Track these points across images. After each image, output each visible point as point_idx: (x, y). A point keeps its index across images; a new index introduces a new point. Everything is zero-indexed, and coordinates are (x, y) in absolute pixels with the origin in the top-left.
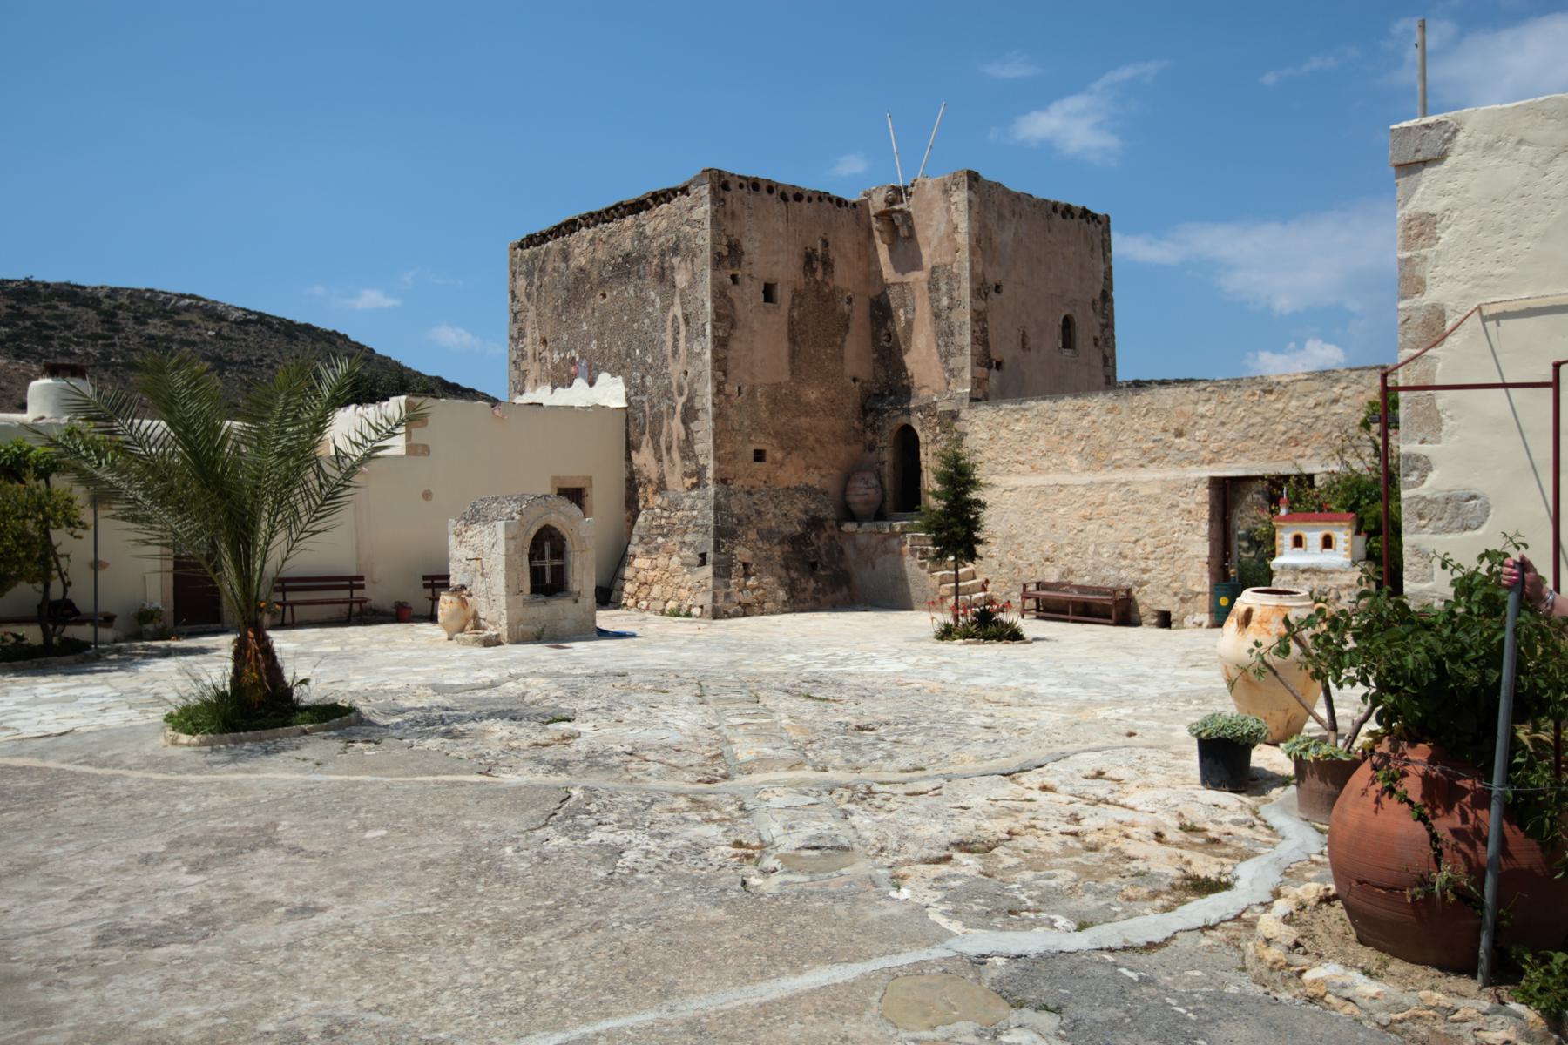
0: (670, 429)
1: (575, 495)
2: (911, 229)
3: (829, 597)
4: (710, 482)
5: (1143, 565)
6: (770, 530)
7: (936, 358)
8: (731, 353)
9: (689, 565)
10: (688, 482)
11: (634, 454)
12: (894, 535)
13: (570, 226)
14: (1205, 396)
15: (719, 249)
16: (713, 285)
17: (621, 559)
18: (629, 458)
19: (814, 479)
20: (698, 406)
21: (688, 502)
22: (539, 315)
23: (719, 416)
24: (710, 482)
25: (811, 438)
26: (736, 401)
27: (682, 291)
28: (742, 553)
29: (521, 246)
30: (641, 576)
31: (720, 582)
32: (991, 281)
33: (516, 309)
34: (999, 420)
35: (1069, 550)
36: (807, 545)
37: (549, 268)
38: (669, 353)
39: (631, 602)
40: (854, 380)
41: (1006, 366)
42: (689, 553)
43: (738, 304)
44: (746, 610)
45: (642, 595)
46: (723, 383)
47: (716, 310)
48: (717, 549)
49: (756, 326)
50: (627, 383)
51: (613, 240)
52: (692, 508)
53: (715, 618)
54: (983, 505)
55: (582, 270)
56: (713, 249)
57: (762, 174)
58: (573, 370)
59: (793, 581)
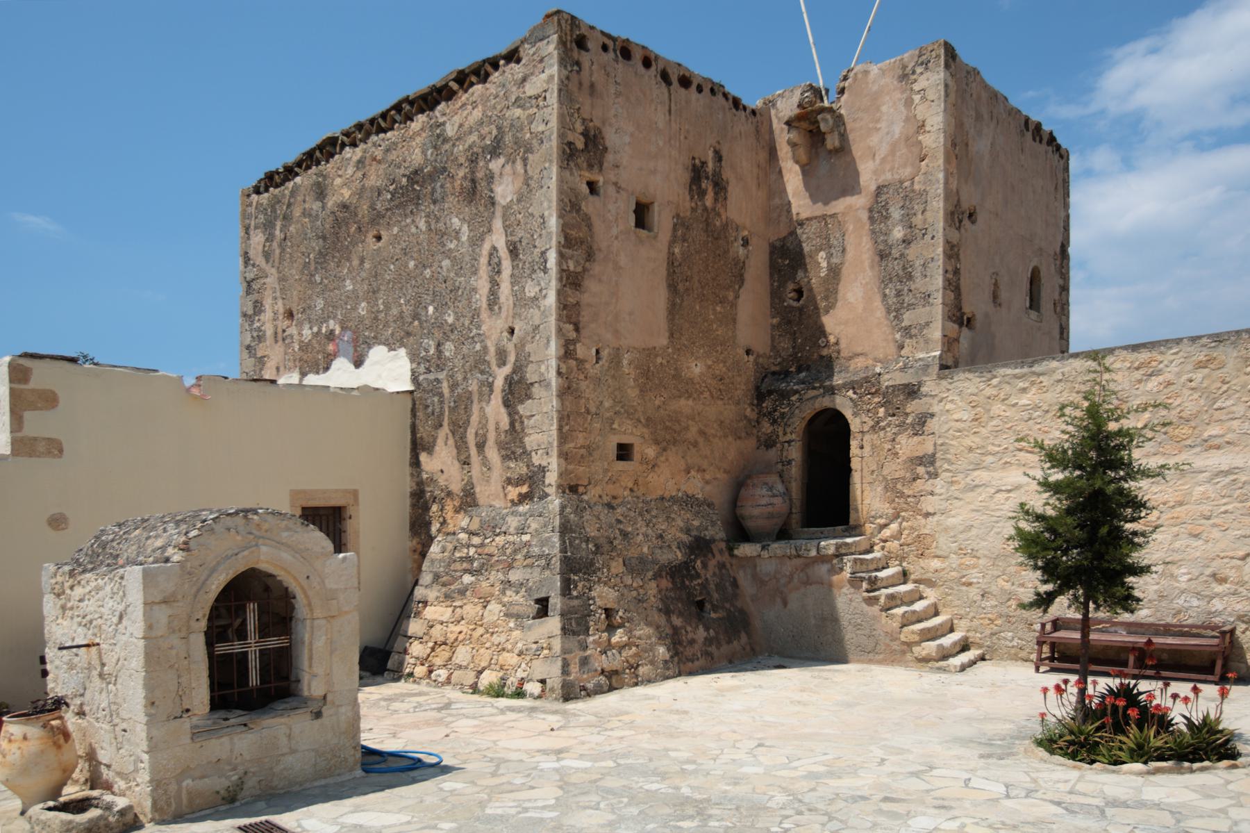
0: (484, 418)
1: (329, 520)
2: (843, 137)
3: (725, 649)
4: (551, 490)
6: (642, 560)
7: (880, 312)
8: (585, 298)
9: (518, 616)
10: (513, 493)
11: (423, 457)
12: (822, 559)
13: (329, 148)
15: (570, 138)
16: (561, 192)
17: (402, 607)
18: (416, 463)
19: (695, 486)
20: (531, 376)
21: (513, 523)
22: (282, 279)
23: (566, 392)
24: (551, 490)
25: (694, 429)
26: (593, 370)
27: (507, 208)
28: (603, 595)
29: (257, 191)
30: (437, 632)
31: (573, 642)
32: (965, 205)
33: (250, 276)
34: (989, 391)
36: (692, 578)
37: (297, 212)
38: (484, 304)
39: (420, 671)
40: (748, 352)
41: (978, 324)
42: (518, 598)
43: (597, 222)
44: (612, 681)
45: (438, 661)
46: (574, 342)
47: (565, 229)
48: (566, 590)
49: (623, 260)
50: (413, 357)
51: (393, 156)
52: (521, 531)
53: (567, 698)
54: (1139, 505)
55: (345, 206)
56: (561, 136)
57: (637, 36)
58: (331, 347)
59: (676, 630)
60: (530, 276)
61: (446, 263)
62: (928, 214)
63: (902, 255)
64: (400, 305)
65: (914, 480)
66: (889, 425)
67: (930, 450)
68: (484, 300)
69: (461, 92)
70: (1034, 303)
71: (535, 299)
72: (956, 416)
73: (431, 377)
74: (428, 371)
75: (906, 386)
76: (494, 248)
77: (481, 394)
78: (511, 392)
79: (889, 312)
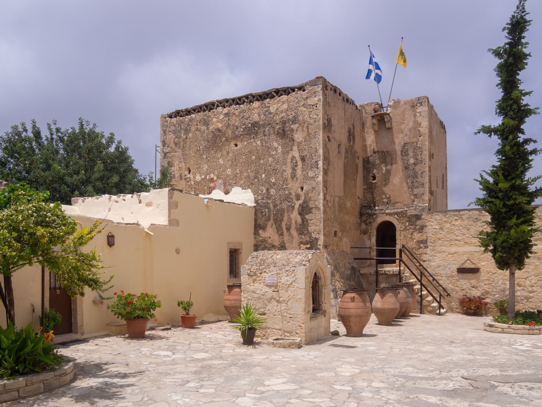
0: (290, 219)
4: (321, 247)
5: (530, 289)
7: (406, 189)
11: (261, 232)
13: (210, 107)
20: (311, 205)
24: (321, 247)
29: (170, 116)
34: (445, 219)
35: (487, 282)
37: (193, 129)
55: (219, 130)
58: (212, 185)
60: (311, 169)
61: (270, 159)
62: (423, 156)
64: (248, 172)
65: (419, 248)
66: (410, 228)
67: (425, 238)
68: (289, 175)
69: (277, 97)
70: (443, 188)
71: (313, 177)
72: (434, 227)
73: (264, 201)
74: (263, 199)
75: (416, 215)
76: (293, 157)
77: (288, 210)
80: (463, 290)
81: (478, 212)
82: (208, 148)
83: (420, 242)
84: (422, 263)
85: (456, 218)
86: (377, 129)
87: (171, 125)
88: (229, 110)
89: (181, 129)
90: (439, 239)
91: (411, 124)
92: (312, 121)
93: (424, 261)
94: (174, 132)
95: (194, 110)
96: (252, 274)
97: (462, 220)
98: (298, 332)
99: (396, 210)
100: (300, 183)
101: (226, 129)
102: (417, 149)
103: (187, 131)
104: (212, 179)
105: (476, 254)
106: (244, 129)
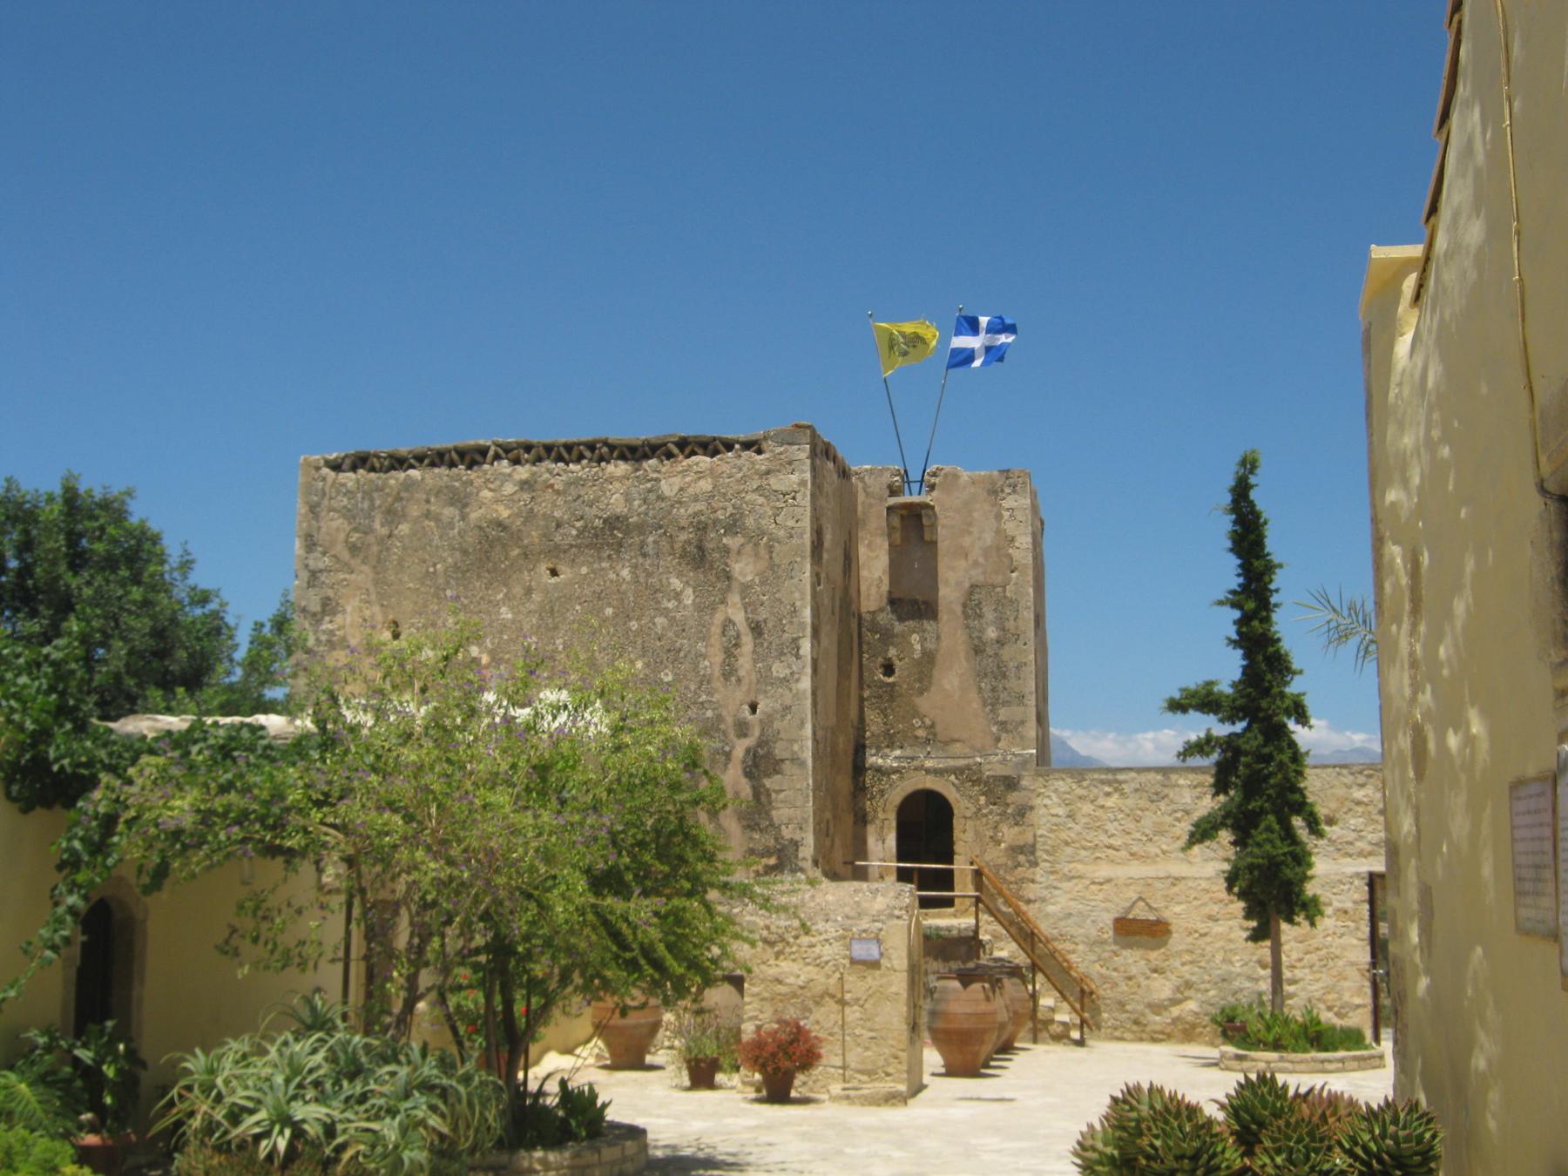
4: (808, 865)
7: (976, 705)
14: (1361, 779)
20: (779, 751)
34: (1080, 792)
35: (1187, 957)
37: (414, 511)
55: (501, 525)
62: (1020, 622)
63: (996, 654)
66: (991, 812)
67: (1030, 840)
71: (785, 680)
72: (1053, 811)
75: (1006, 778)
76: (728, 623)
78: (755, 765)
79: (985, 705)
80: (1130, 978)
81: (1159, 777)
82: (464, 573)
83: (1017, 850)
84: (1024, 907)
85: (1107, 789)
86: (898, 542)
87: (338, 492)
88: (533, 474)
89: (372, 507)
90: (1067, 844)
91: (988, 538)
92: (782, 533)
93: (1029, 902)
94: (348, 514)
95: (420, 458)
96: (773, 938)
97: (1123, 794)
98: (890, 1070)
99: (951, 763)
100: (749, 690)
101: (524, 523)
102: (1005, 604)
103: (393, 516)
104: (476, 661)
105: (1158, 885)
106: (581, 532)
